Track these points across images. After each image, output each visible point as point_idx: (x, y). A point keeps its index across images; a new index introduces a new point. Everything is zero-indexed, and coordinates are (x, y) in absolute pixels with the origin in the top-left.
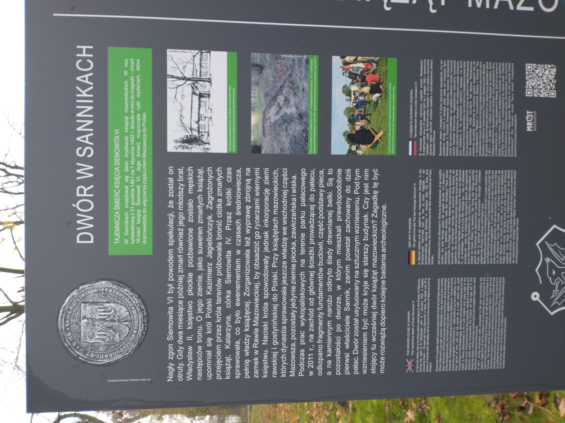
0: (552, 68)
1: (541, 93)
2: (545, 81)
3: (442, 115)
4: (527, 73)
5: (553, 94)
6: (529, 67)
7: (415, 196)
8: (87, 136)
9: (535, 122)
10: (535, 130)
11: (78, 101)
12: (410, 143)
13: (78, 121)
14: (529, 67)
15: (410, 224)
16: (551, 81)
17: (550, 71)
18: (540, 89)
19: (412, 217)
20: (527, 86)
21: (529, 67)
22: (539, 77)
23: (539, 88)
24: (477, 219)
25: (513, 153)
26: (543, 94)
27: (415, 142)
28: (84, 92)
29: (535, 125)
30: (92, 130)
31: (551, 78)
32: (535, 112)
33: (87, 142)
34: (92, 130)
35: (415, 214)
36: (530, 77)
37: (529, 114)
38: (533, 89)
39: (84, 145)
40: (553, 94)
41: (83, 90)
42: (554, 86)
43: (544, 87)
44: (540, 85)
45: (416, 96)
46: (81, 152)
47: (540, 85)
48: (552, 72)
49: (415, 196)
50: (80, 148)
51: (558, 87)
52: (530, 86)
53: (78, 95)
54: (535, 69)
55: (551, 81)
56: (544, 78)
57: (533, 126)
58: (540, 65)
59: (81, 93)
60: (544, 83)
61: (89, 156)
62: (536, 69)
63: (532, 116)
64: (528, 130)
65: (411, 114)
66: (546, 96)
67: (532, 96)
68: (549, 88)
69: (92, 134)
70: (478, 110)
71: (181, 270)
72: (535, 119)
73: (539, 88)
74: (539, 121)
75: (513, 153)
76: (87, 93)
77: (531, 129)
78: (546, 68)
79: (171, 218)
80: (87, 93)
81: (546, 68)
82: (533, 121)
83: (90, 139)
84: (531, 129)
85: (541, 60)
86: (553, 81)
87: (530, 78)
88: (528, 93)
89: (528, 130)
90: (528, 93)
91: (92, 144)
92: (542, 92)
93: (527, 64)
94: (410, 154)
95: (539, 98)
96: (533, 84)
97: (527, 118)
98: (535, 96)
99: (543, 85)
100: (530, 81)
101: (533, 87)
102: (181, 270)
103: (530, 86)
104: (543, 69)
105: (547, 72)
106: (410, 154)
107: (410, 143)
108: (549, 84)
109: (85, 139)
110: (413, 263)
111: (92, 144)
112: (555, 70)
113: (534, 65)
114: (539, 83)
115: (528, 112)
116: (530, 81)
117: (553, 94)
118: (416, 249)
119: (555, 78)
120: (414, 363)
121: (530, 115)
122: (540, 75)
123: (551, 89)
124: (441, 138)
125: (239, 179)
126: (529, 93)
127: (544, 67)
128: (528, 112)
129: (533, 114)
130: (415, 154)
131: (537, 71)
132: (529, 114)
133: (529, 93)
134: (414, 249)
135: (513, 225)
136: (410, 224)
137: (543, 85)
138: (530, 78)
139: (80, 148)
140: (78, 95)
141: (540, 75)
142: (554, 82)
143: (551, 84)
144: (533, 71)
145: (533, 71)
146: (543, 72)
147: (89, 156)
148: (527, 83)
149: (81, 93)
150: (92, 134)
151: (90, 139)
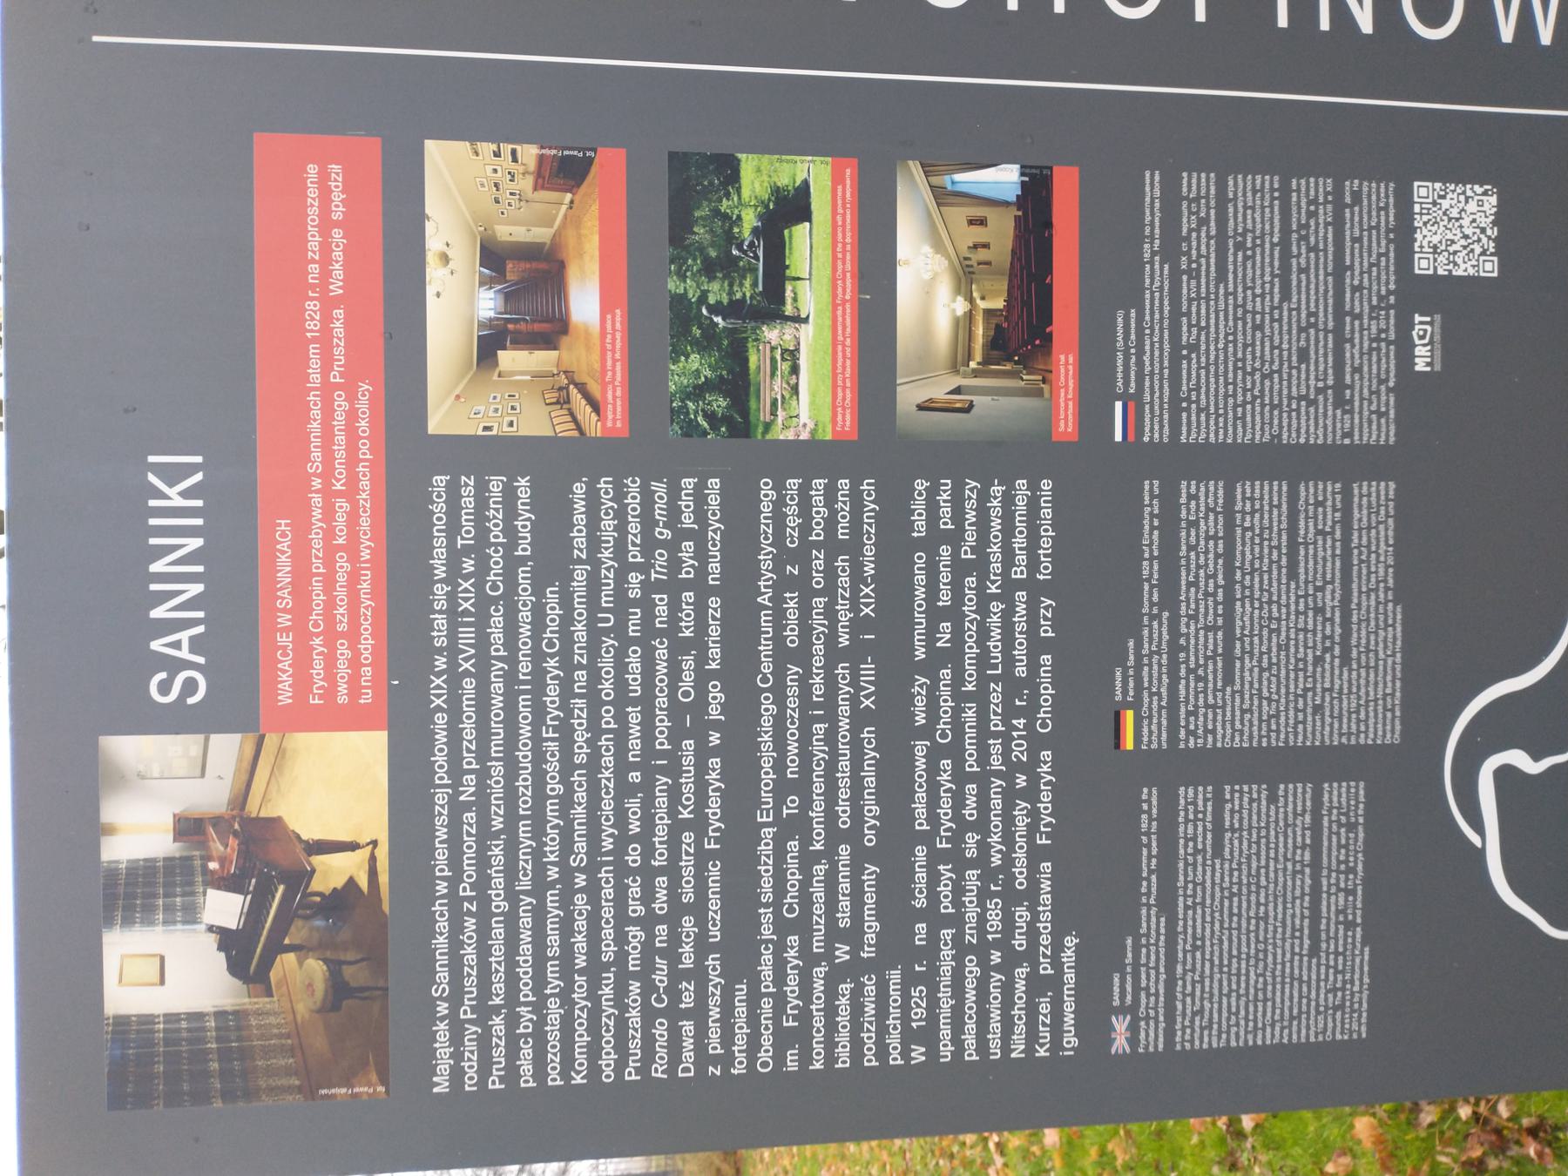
0: (1485, 193)
1: (1455, 264)
2: (1468, 231)
3: (1216, 603)
4: (1417, 208)
5: (1490, 268)
6: (1423, 190)
7: (1130, 955)
8: (184, 636)
9: (1438, 346)
10: (1438, 368)
11: (153, 522)
12: (1119, 405)
13: (154, 587)
14: (1423, 192)
15: (1118, 684)
16: (1483, 230)
17: (1480, 204)
18: (1455, 253)
19: (1122, 661)
20: (1417, 245)
21: (1423, 190)
22: (1450, 219)
23: (1451, 249)
24: (1288, 629)
25: (1382, 433)
26: (1463, 266)
27: (1131, 405)
28: (172, 492)
29: (1438, 353)
30: (201, 614)
31: (1485, 222)
32: (1438, 317)
33: (184, 653)
34: (201, 614)
35: (1129, 960)
36: (1425, 218)
37: (1421, 323)
38: (1435, 252)
39: (177, 665)
40: (1490, 268)
41: (171, 485)
42: (1492, 244)
43: (1465, 247)
44: (1453, 242)
45: (1133, 337)
46: (165, 688)
47: (1453, 242)
48: (1486, 207)
49: (1130, 955)
50: (163, 675)
51: (1503, 248)
52: (1425, 243)
53: (152, 503)
54: (1441, 197)
55: (1483, 230)
56: (1466, 222)
57: (1432, 357)
58: (1452, 187)
59: (167, 497)
60: (1466, 237)
61: (191, 701)
62: (1443, 197)
63: (1428, 328)
64: (1417, 368)
65: (1120, 375)
66: (1471, 271)
67: (1431, 272)
68: (1478, 250)
69: (201, 629)
70: (1293, 314)
71: (581, 655)
72: (1437, 338)
73: (1451, 249)
74: (1449, 343)
75: (1382, 433)
76: (184, 494)
77: (1428, 364)
78: (1469, 193)
79: (525, 605)
80: (184, 494)
81: (1469, 193)
82: (1431, 343)
83: (196, 645)
84: (1428, 364)
85: (1455, 170)
86: (1489, 232)
87: (1425, 224)
88: (1422, 266)
89: (1417, 368)
90: (1422, 266)
91: (201, 660)
92: (1459, 261)
93: (1416, 184)
94: (1118, 437)
95: (1450, 277)
96: (1435, 239)
97: (1414, 333)
98: (1440, 272)
99: (1463, 242)
100: (1425, 232)
101: (1435, 247)
102: (581, 655)
103: (1425, 243)
104: (1462, 198)
105: (1472, 206)
106: (1118, 437)
107: (1119, 405)
108: (1479, 240)
109: (179, 645)
110: (1129, 744)
111: (201, 660)
112: (1494, 200)
113: (1438, 185)
114: (1450, 236)
115: (1417, 318)
116: (1425, 232)
117: (1488, 266)
118: (1136, 705)
119: (1494, 223)
120: (1133, 1028)
121: (1422, 325)
122: (1454, 213)
123: (1484, 253)
124: (1185, 189)
125: (608, 793)
126: (1424, 264)
127: (1464, 193)
128: (1417, 318)
129: (1431, 323)
130: (1131, 438)
131: (1445, 204)
132: (1421, 323)
133: (1424, 264)
134: (1129, 706)
135: (1383, 633)
136: (1118, 684)
137: (1463, 242)
138: (1425, 224)
139: (163, 675)
140: (152, 503)
141: (1454, 213)
142: (1493, 232)
143: (1484, 240)
144: (1434, 203)
145: (1434, 203)
146: (1461, 206)
147: (191, 701)
148: (1418, 236)
149: (167, 497)
150: (201, 629)
151: (196, 645)
